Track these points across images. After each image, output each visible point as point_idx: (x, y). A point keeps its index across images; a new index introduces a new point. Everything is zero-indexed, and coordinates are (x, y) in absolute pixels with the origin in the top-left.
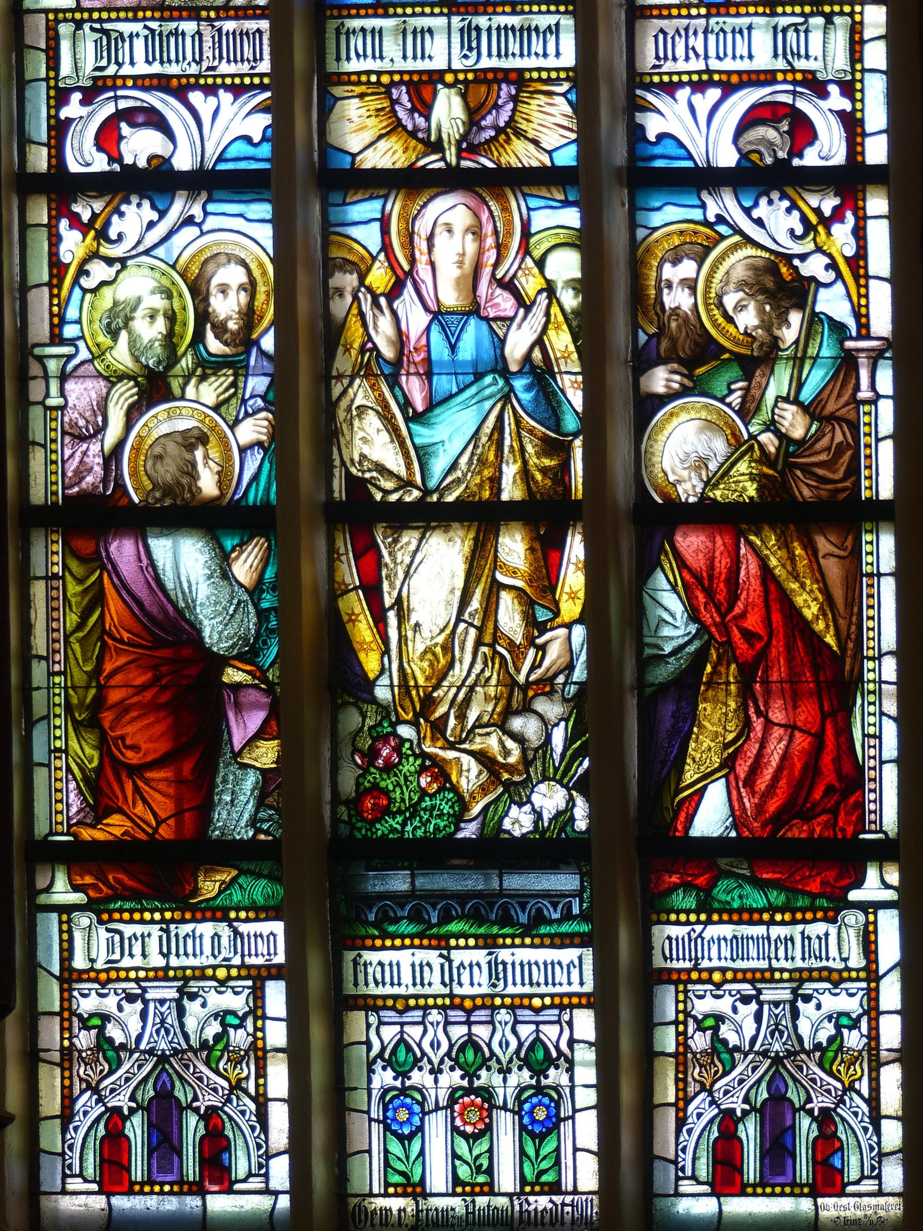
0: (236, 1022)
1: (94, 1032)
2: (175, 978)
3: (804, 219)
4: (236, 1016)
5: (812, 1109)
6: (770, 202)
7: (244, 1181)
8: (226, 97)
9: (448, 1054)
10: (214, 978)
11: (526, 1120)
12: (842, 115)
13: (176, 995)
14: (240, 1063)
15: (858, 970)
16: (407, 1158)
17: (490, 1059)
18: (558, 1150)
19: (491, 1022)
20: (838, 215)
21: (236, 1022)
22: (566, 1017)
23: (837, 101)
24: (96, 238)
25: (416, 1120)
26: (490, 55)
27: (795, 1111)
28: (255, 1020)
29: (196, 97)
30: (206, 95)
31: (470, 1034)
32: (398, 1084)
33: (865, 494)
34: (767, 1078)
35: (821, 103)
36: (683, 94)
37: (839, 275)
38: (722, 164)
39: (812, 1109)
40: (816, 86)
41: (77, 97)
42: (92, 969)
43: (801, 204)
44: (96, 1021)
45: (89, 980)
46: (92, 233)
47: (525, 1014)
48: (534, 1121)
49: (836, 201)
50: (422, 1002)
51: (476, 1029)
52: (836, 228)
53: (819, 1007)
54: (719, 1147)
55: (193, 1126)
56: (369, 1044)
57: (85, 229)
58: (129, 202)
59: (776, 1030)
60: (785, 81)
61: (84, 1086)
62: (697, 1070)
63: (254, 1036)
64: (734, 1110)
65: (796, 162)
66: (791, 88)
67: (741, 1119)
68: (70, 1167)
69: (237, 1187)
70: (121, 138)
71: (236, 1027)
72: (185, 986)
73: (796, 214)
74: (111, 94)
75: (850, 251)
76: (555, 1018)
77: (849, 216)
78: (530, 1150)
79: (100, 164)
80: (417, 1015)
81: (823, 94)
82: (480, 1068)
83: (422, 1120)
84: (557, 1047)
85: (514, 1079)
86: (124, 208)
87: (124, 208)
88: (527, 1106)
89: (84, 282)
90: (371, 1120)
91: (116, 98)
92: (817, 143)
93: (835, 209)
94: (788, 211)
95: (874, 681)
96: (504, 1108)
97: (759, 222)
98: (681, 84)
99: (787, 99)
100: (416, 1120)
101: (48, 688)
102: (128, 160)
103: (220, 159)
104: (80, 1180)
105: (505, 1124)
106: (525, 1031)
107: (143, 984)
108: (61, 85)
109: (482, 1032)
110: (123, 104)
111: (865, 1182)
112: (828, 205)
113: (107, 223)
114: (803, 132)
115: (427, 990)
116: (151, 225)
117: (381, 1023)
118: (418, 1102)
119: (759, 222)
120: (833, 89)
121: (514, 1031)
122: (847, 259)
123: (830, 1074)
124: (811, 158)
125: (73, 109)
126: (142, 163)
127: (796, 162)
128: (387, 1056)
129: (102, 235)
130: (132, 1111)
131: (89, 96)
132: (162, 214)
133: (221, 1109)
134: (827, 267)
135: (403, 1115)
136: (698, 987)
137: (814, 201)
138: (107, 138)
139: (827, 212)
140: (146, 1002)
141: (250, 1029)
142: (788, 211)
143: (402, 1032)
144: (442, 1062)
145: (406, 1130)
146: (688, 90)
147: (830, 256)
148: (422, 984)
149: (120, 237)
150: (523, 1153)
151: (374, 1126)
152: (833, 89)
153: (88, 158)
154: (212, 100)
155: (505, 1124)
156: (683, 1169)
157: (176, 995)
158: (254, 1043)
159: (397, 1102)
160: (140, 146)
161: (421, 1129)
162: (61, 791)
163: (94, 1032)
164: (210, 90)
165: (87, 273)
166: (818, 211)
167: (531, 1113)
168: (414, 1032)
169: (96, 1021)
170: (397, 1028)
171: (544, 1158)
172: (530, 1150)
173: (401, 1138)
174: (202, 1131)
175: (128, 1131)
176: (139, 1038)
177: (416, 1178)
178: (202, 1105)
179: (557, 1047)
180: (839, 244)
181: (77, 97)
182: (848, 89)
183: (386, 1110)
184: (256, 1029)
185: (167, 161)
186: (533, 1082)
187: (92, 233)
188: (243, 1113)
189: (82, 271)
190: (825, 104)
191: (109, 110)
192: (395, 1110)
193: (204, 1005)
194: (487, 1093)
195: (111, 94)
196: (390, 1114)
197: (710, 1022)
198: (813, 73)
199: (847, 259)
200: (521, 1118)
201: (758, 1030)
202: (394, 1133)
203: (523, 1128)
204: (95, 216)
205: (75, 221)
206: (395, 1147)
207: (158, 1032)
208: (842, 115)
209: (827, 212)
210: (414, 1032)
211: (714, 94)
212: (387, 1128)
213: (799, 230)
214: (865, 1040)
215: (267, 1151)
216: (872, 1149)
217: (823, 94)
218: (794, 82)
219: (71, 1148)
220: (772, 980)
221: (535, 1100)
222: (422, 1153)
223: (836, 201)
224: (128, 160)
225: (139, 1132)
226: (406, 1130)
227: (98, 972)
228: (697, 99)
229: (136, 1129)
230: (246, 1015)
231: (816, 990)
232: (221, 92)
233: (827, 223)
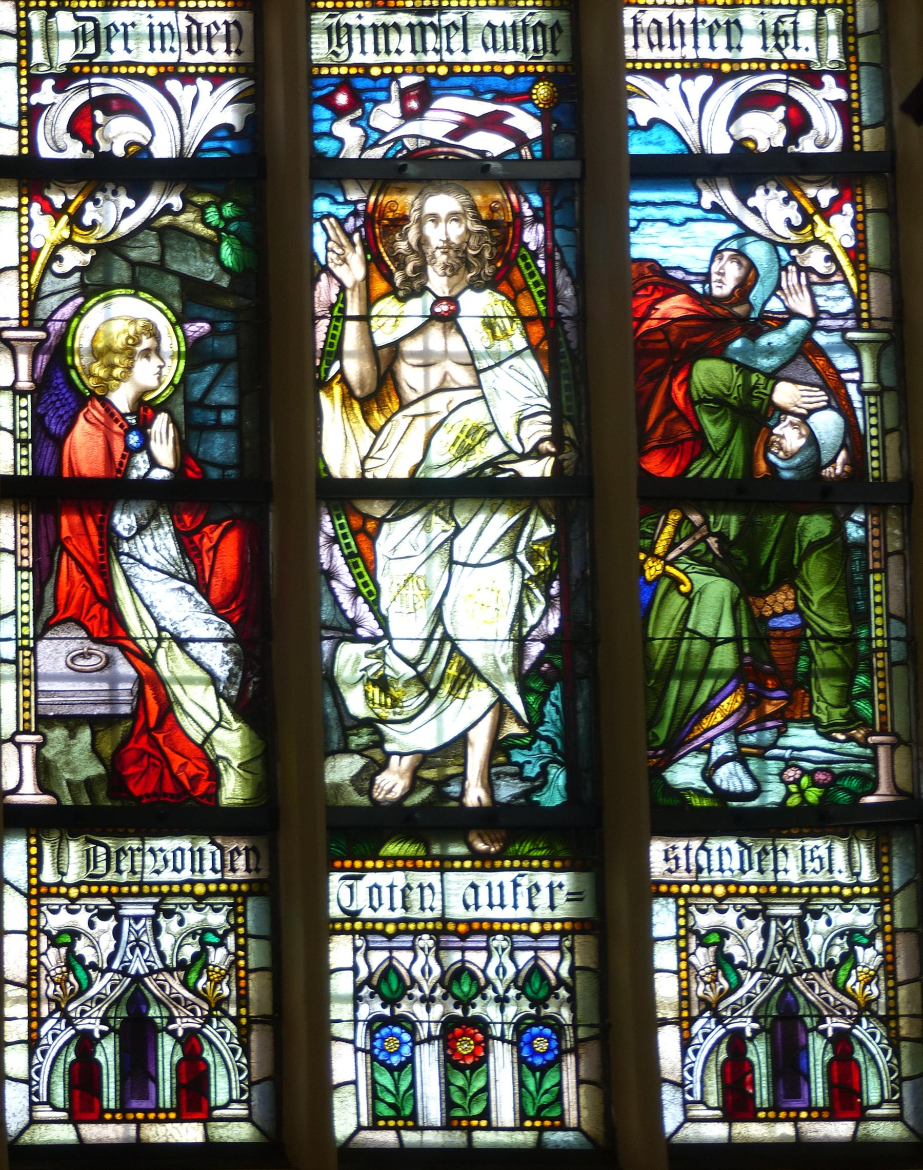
0: (216, 940)
1: (63, 950)
2: (151, 894)
3: (801, 209)
4: (216, 934)
5: (826, 1030)
6: (767, 191)
7: (225, 1107)
8: (204, 85)
9: (441, 981)
10: (191, 894)
11: (525, 1053)
12: (837, 104)
13: (152, 912)
14: (220, 982)
15: (870, 885)
16: (397, 1089)
17: (486, 987)
18: (560, 1084)
19: (487, 949)
20: (835, 206)
21: (216, 940)
22: (567, 943)
23: (832, 91)
24: (70, 224)
25: (406, 1050)
26: (501, 886)
27: (808, 1031)
28: (237, 936)
29: (173, 85)
30: (184, 85)
31: (463, 961)
32: (387, 1012)
33: (857, 147)
34: (777, 995)
35: (815, 92)
36: (674, 81)
37: (839, 268)
38: (716, 151)
39: (826, 1030)
40: (809, 76)
41: (48, 84)
42: (60, 884)
43: (797, 193)
44: (67, 939)
45: (58, 895)
46: (65, 219)
47: (521, 940)
48: (534, 1053)
49: (834, 192)
50: (412, 926)
51: (469, 955)
52: (835, 219)
53: (829, 922)
54: (728, 1070)
55: (168, 1052)
56: (355, 969)
57: (57, 214)
58: (104, 190)
59: (785, 946)
60: (780, 71)
61: (53, 1006)
62: (702, 986)
63: (235, 954)
64: (743, 1030)
65: (792, 149)
66: (784, 77)
67: (751, 1039)
68: (37, 1094)
69: (217, 1113)
70: (96, 126)
71: (216, 946)
72: (161, 902)
73: (793, 203)
74: (86, 81)
75: (850, 243)
76: (556, 944)
77: (847, 208)
78: (531, 1083)
79: (74, 150)
80: (407, 940)
81: (819, 85)
82: (475, 997)
83: (412, 1050)
84: (557, 974)
85: (511, 1011)
86: (99, 196)
87: (99, 196)
88: (526, 1037)
89: (56, 267)
90: (357, 1050)
91: (89, 86)
92: (812, 133)
93: (833, 200)
94: (786, 201)
95: (882, 638)
96: (502, 1039)
97: (755, 211)
98: (672, 71)
99: (781, 88)
100: (406, 1050)
101: (17, 639)
102: (103, 147)
103: (199, 149)
104: (48, 1108)
105: (502, 1060)
106: (524, 958)
107: (117, 900)
108: (33, 72)
109: (477, 959)
110: (97, 92)
111: (885, 1106)
112: (826, 195)
113: (81, 210)
114: (798, 123)
115: (394, 58)
116: (127, 212)
117: (368, 949)
118: (408, 1031)
119: (755, 211)
120: (828, 80)
121: (512, 958)
122: (847, 251)
123: (843, 991)
124: (807, 145)
125: (46, 94)
126: (119, 151)
127: (792, 149)
128: (375, 981)
129: (76, 220)
130: (103, 1034)
131: (63, 82)
132: (139, 203)
133: (199, 1031)
134: (827, 259)
135: (391, 1045)
136: (702, 901)
137: (811, 192)
138: (81, 126)
139: (824, 202)
140: (120, 919)
141: (232, 947)
142: (786, 201)
143: (391, 958)
144: (433, 990)
145: (395, 1060)
146: (677, 77)
147: (827, 247)
148: (388, 52)
149: (94, 224)
150: (522, 1084)
151: (361, 1055)
152: (828, 80)
153: (62, 146)
154: (190, 90)
155: (502, 1060)
156: (690, 1092)
157: (152, 912)
158: (234, 963)
159: (384, 1031)
160: (118, 134)
161: (411, 1060)
162: (22, 536)
163: (63, 950)
164: (188, 79)
165: (60, 259)
166: (814, 201)
167: (530, 1044)
168: (404, 957)
169: (67, 939)
170: (386, 954)
171: (546, 1092)
172: (531, 1083)
173: (391, 1069)
174: (179, 1055)
175: (99, 1056)
176: (111, 958)
177: (407, 1111)
178: (180, 1026)
179: (557, 974)
180: (838, 235)
181: (48, 84)
182: (842, 79)
183: (373, 1039)
184: (238, 947)
185: (145, 148)
186: (533, 1011)
187: (65, 219)
188: (223, 1035)
189: (54, 257)
190: (821, 94)
191: (83, 97)
192: (383, 1039)
193: (181, 923)
194: (482, 1024)
195: (86, 81)
196: (377, 1043)
197: (714, 938)
198: (807, 63)
199: (847, 251)
200: (519, 1051)
201: (765, 945)
202: (382, 1063)
203: (521, 1061)
204: (68, 203)
205: (49, 209)
206: (385, 1079)
207: (132, 952)
208: (837, 104)
209: (824, 202)
210: (404, 957)
211: (705, 81)
212: (374, 1058)
213: (797, 220)
214: (880, 958)
215: (248, 1076)
216: (892, 1072)
217: (819, 85)
218: (789, 72)
219: (38, 1073)
220: (779, 894)
221: (535, 1030)
222: (413, 1085)
223: (834, 192)
224: (103, 147)
225: (111, 1058)
226: (395, 1060)
227: (69, 886)
228: (688, 85)
229: (107, 1054)
230: (226, 933)
231: (826, 905)
232: (199, 80)
233: (826, 215)
